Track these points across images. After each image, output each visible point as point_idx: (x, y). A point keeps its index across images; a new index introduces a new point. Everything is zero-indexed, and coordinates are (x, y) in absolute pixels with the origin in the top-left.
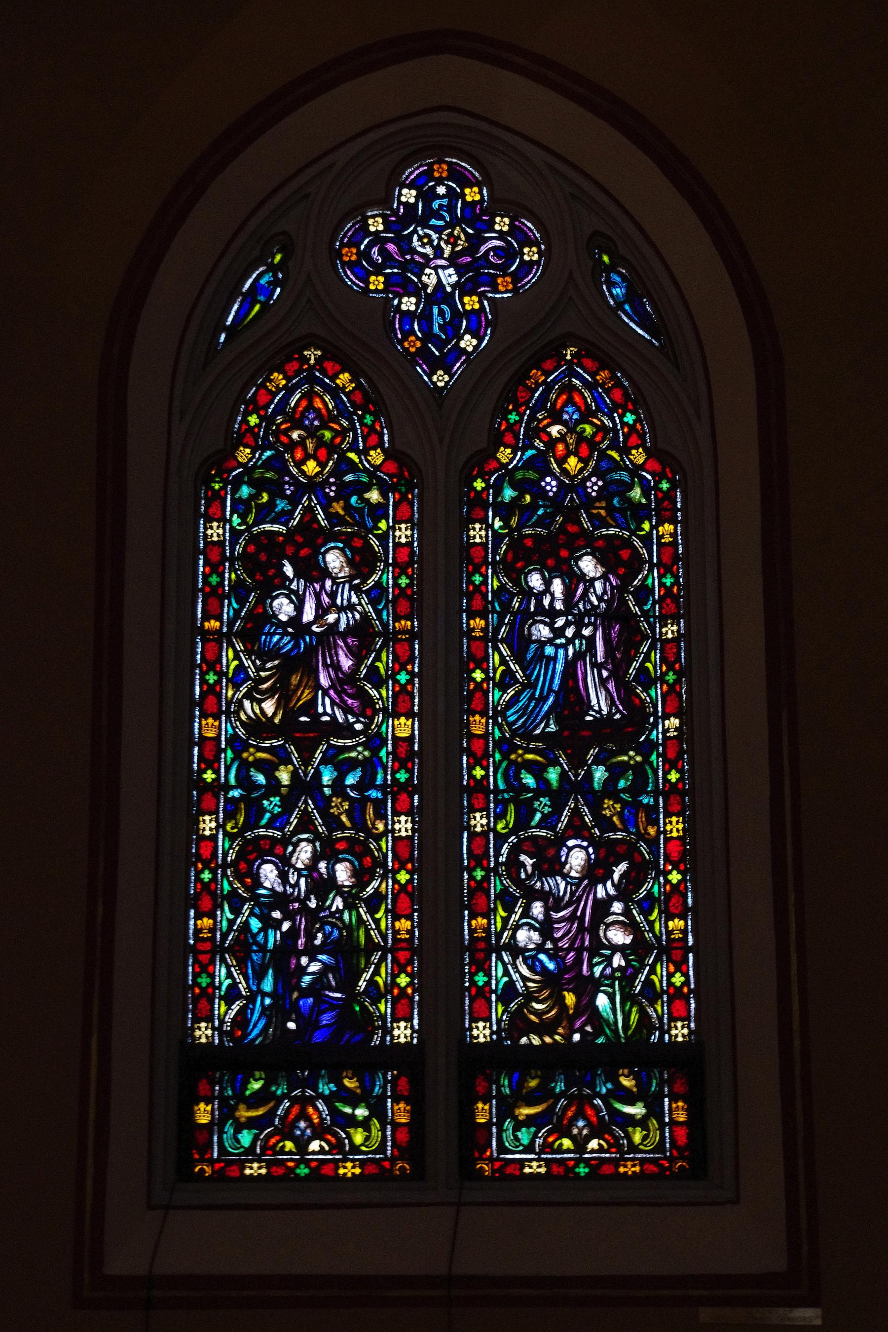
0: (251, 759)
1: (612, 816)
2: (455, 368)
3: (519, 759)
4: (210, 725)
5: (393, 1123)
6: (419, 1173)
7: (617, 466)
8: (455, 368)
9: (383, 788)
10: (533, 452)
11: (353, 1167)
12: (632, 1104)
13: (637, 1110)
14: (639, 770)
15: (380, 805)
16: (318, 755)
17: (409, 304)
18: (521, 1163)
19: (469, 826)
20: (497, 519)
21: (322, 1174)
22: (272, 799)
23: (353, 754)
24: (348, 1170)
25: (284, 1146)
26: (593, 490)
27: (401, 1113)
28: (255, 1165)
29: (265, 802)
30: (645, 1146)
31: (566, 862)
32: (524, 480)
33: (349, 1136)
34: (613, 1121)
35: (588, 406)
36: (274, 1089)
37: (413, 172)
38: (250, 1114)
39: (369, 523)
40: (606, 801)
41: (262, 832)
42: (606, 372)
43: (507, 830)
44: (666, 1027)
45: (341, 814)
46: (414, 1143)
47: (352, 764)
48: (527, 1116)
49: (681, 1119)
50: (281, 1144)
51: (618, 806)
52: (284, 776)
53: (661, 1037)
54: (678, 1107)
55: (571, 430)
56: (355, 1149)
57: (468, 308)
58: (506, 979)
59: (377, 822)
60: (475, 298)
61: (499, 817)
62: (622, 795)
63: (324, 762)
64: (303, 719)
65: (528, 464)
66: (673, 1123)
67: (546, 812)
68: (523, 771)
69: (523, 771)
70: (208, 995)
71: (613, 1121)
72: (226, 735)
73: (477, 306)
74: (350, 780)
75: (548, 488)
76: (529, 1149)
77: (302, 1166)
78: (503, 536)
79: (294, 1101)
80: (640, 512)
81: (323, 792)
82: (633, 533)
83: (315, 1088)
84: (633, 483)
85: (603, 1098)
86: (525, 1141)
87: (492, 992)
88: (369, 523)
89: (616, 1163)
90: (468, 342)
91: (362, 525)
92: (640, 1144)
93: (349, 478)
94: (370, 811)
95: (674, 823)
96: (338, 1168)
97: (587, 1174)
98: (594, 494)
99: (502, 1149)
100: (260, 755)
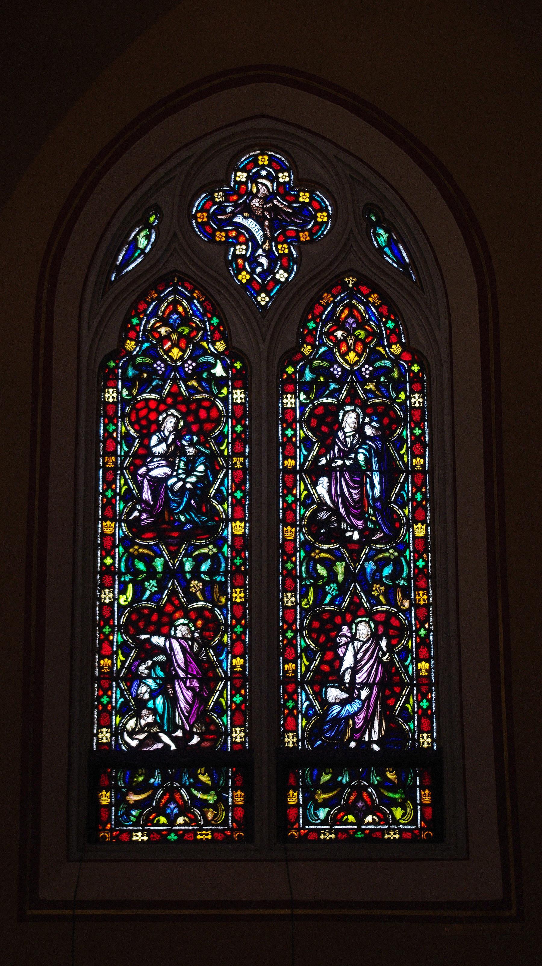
1: (379, 595)
5: (421, 804)
6: (249, 839)
11: (394, 834)
12: (395, 792)
15: (223, 586)
16: (182, 551)
20: (302, 393)
21: (374, 838)
23: (387, 554)
25: (159, 821)
26: (189, 369)
27: (423, 796)
29: (146, 583)
30: (404, 820)
32: (319, 367)
33: (391, 813)
36: (340, 779)
37: (244, 160)
40: (375, 586)
41: (144, 604)
45: (379, 595)
46: (247, 818)
47: (202, 558)
48: (135, 801)
50: (345, 817)
51: (383, 588)
53: (413, 744)
54: (425, 794)
56: (396, 822)
59: (404, 601)
60: (286, 246)
64: (322, 531)
65: (145, 353)
67: (153, 591)
71: (194, 805)
72: (300, 541)
74: (204, 567)
75: (335, 372)
76: (324, 822)
83: (368, 781)
85: (375, 787)
89: (195, 832)
90: (281, 276)
92: (400, 819)
94: (216, 587)
95: (238, 597)
97: (175, 840)
98: (367, 376)
99: (307, 822)
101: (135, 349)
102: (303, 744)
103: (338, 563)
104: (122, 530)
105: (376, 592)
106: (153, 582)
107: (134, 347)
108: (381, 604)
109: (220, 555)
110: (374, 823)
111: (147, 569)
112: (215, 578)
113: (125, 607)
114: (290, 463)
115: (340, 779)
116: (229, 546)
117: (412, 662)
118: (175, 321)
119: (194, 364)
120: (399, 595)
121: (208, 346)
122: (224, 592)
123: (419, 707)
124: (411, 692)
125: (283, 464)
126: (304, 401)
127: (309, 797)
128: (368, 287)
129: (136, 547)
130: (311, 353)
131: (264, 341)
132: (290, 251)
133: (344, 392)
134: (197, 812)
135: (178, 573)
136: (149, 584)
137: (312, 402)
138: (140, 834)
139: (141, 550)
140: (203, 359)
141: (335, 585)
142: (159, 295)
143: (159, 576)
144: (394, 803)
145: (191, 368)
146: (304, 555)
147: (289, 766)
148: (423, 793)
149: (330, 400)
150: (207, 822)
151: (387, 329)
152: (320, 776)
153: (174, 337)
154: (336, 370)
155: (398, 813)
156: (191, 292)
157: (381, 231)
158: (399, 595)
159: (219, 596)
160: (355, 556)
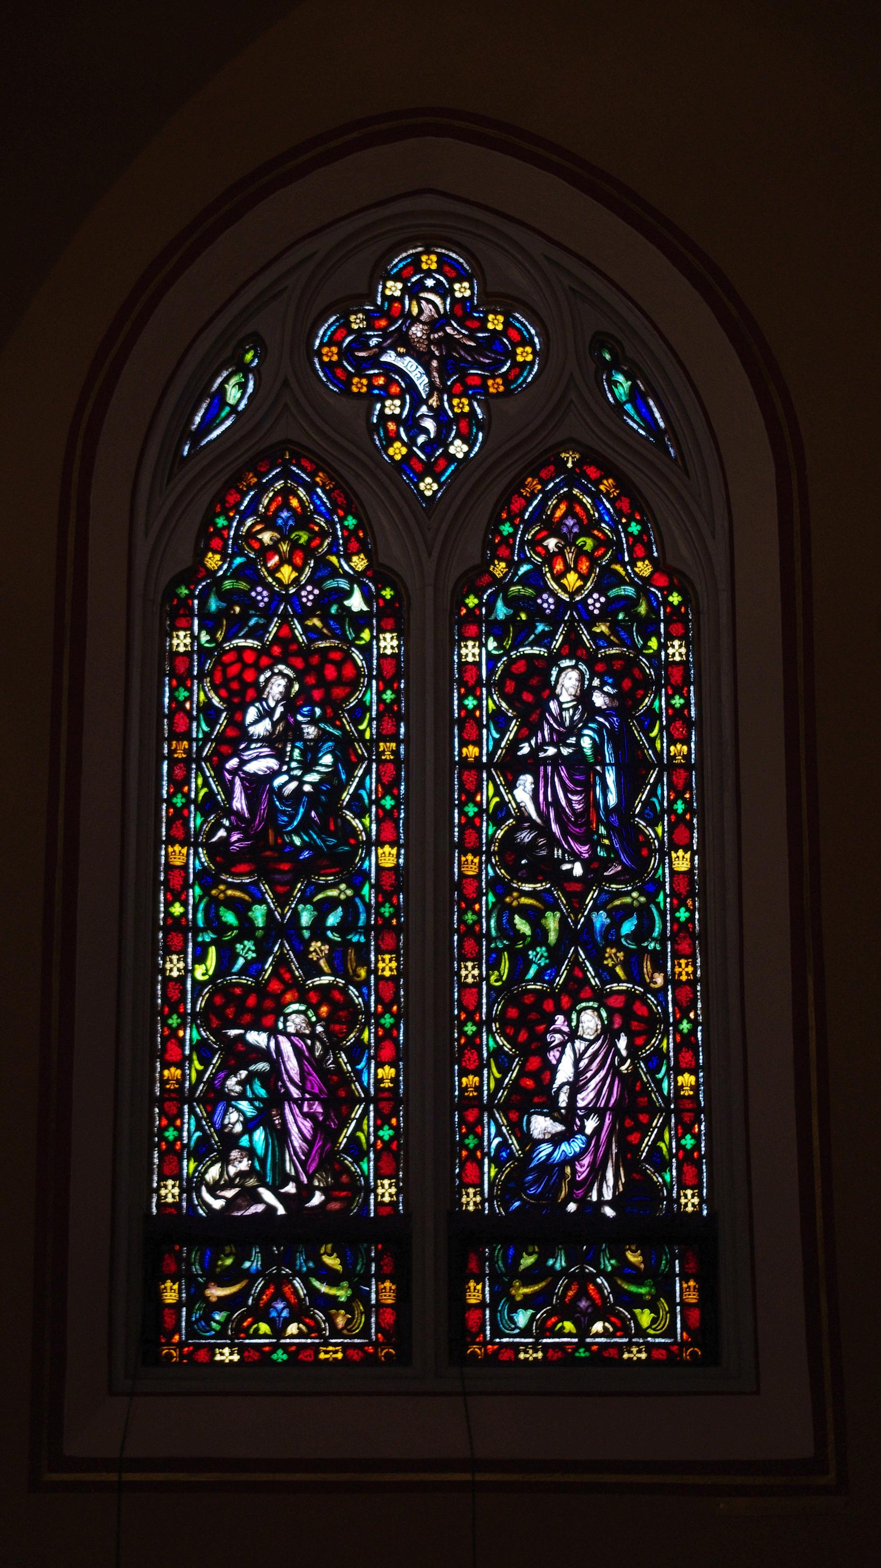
1: (614, 966)
4: (469, 861)
5: (683, 1303)
6: (403, 1358)
9: (367, 930)
12: (640, 1284)
13: (342, 1294)
18: (515, 1347)
19: (164, 970)
20: (491, 639)
21: (608, 1358)
24: (332, 1353)
30: (654, 1329)
33: (634, 1317)
34: (618, 1301)
36: (551, 1262)
37: (398, 262)
39: (640, 642)
40: (608, 950)
41: (234, 979)
46: (400, 1325)
48: (219, 1298)
49: (390, 1301)
50: (255, 1326)
51: (621, 955)
54: (689, 1287)
55: (284, 538)
56: (641, 1332)
59: (656, 975)
66: (379, 1305)
67: (249, 958)
70: (474, 1159)
73: (467, 409)
74: (332, 920)
75: (545, 605)
76: (525, 1332)
78: (499, 657)
79: (572, 1277)
85: (608, 1276)
87: (484, 1155)
88: (640, 642)
89: (315, 1348)
90: (458, 449)
91: (343, 638)
92: (648, 1328)
99: (497, 1332)
101: (220, 568)
102: (491, 1207)
106: (249, 944)
107: (220, 563)
108: (619, 981)
109: (358, 900)
110: (301, 1335)
112: (349, 937)
113: (204, 984)
114: (471, 751)
116: (371, 886)
117: (667, 1073)
118: (286, 521)
120: (647, 966)
123: (680, 1147)
124: (667, 1122)
125: (460, 753)
127: (501, 1291)
131: (430, 555)
133: (560, 638)
134: (320, 1315)
135: (290, 929)
136: (242, 946)
137: (507, 653)
138: (226, 1351)
139: (229, 892)
141: (544, 949)
142: (260, 479)
143: (259, 933)
144: (638, 1302)
145: (311, 597)
146: (494, 900)
147: (468, 1242)
148: (685, 1285)
149: (536, 650)
150: (336, 1332)
155: (645, 1318)
156: (312, 475)
157: (620, 378)
158: (647, 966)
159: (356, 967)
160: (576, 903)
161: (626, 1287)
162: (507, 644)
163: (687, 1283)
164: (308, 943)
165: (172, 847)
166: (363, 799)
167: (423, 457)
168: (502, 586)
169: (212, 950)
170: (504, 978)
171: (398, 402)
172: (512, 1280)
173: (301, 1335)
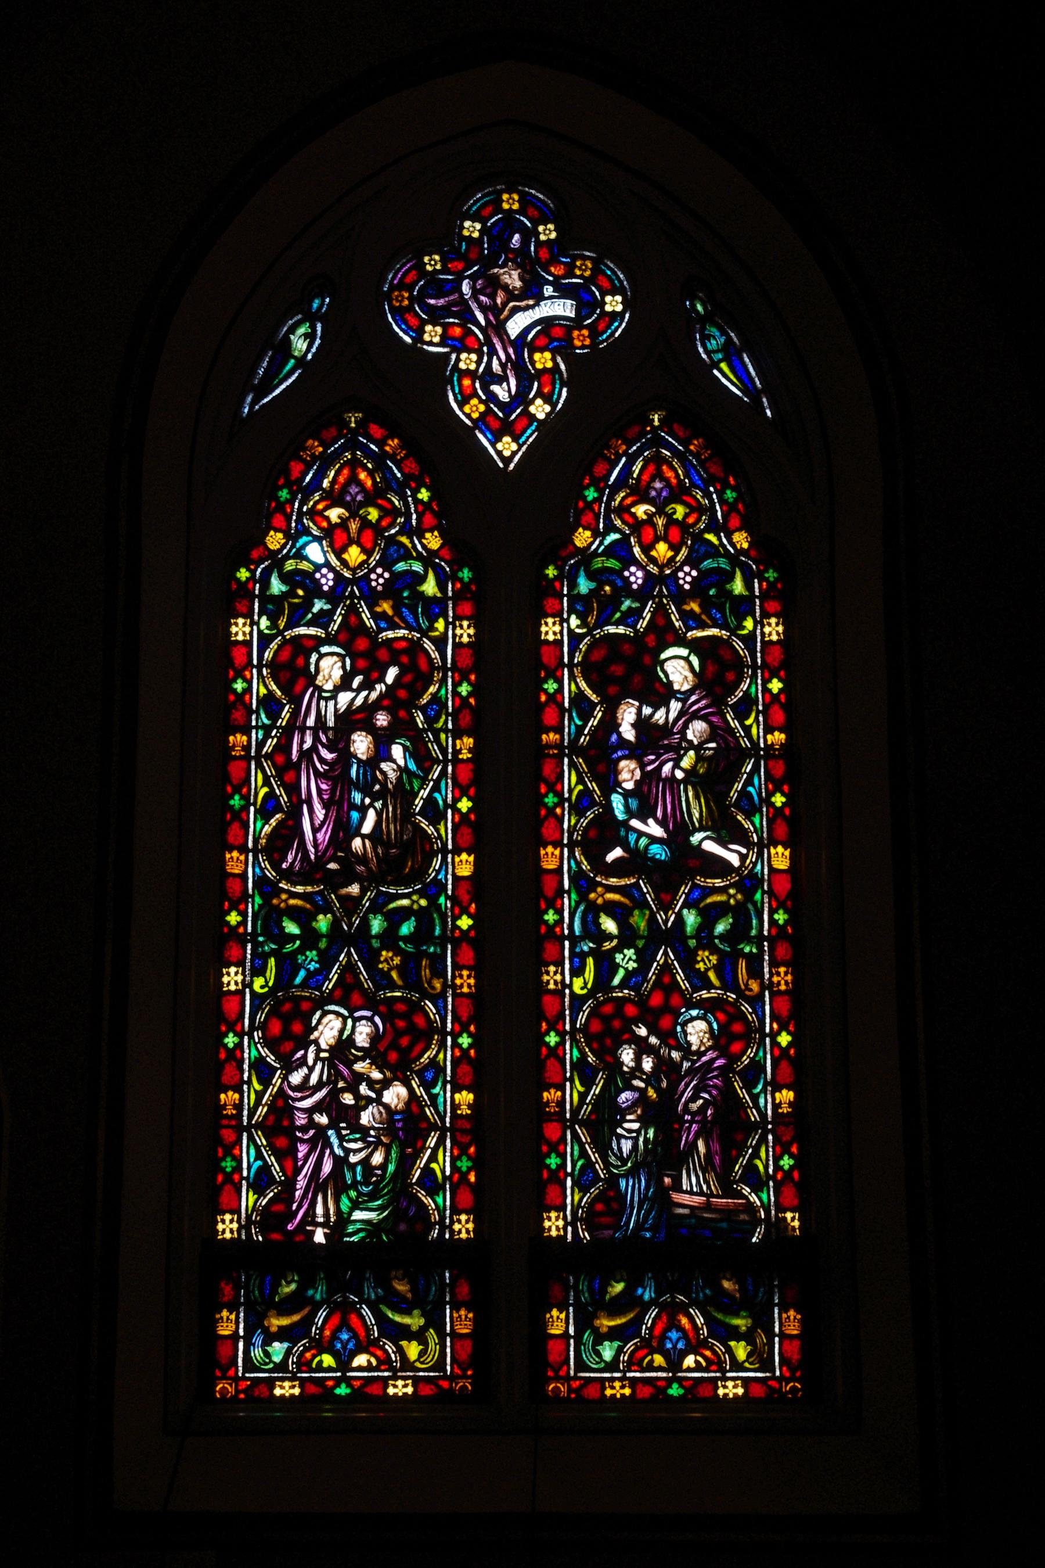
0: (600, 901)
1: (707, 970)
2: (534, 436)
3: (732, 901)
5: (453, 1334)
7: (714, 551)
8: (534, 436)
10: (617, 536)
11: (735, 1387)
12: (408, 1312)
13: (414, 1321)
14: (423, 917)
17: (468, 361)
21: (370, 1394)
22: (626, 951)
24: (400, 1388)
28: (287, 1384)
30: (422, 1363)
31: (316, 1028)
33: (730, 1351)
35: (680, 482)
38: (612, 1323)
40: (700, 953)
42: (396, 441)
43: (266, 989)
44: (447, 1221)
45: (390, 969)
50: (649, 1357)
52: (639, 921)
53: (441, 1233)
55: (660, 511)
57: (539, 366)
58: (259, 1163)
61: (259, 971)
62: (401, 943)
63: (686, 905)
67: (630, 969)
68: (602, 914)
69: (284, 918)
73: (549, 365)
74: (406, 929)
76: (612, 1366)
77: (343, 1386)
78: (582, 636)
79: (663, 1307)
80: (434, 608)
81: (370, 944)
82: (733, 632)
84: (734, 573)
86: (277, 1358)
93: (401, 566)
94: (742, 965)
96: (386, 1386)
98: (379, 588)
99: (581, 1366)
100: (610, 896)
102: (575, 1232)
103: (321, 917)
104: (259, 863)
105: (701, 964)
106: (630, 953)
107: (283, 541)
108: (394, 987)
109: (750, 906)
110: (698, 1367)
111: (619, 932)
113: (583, 999)
115: (311, 1292)
116: (763, 892)
117: (764, 1090)
118: (659, 492)
119: (694, 573)
120: (426, 973)
121: (720, 539)
122: (755, 972)
123: (777, 1168)
124: (441, 1142)
125: (765, 740)
126: (578, 631)
127: (584, 1322)
128: (382, 425)
129: (284, 896)
130: (284, 546)
132: (556, 365)
133: (647, 615)
134: (390, 1348)
136: (622, 956)
137: (281, 633)
140: (708, 564)
141: (314, 952)
143: (323, 944)
144: (403, 1333)
145: (381, 581)
146: (261, 902)
148: (455, 1315)
149: (621, 630)
150: (737, 1366)
151: (417, 501)
152: (605, 1285)
153: (660, 522)
154: (634, 574)
155: (413, 1350)
158: (426, 973)
159: (431, 979)
161: (390, 1316)
162: (591, 620)
163: (457, 1312)
164: (694, 953)
165: (775, 848)
166: (753, 797)
167: (501, 415)
168: (586, 556)
169: (590, 961)
170: (589, 986)
171: (474, 357)
172: (268, 1309)
173: (698, 1367)
